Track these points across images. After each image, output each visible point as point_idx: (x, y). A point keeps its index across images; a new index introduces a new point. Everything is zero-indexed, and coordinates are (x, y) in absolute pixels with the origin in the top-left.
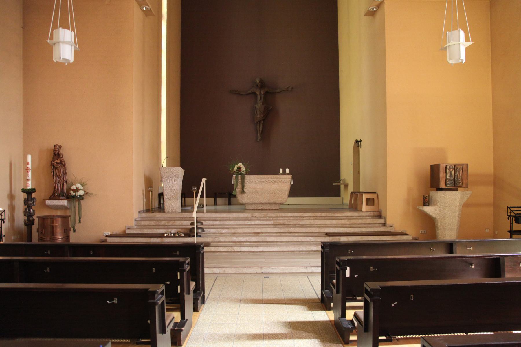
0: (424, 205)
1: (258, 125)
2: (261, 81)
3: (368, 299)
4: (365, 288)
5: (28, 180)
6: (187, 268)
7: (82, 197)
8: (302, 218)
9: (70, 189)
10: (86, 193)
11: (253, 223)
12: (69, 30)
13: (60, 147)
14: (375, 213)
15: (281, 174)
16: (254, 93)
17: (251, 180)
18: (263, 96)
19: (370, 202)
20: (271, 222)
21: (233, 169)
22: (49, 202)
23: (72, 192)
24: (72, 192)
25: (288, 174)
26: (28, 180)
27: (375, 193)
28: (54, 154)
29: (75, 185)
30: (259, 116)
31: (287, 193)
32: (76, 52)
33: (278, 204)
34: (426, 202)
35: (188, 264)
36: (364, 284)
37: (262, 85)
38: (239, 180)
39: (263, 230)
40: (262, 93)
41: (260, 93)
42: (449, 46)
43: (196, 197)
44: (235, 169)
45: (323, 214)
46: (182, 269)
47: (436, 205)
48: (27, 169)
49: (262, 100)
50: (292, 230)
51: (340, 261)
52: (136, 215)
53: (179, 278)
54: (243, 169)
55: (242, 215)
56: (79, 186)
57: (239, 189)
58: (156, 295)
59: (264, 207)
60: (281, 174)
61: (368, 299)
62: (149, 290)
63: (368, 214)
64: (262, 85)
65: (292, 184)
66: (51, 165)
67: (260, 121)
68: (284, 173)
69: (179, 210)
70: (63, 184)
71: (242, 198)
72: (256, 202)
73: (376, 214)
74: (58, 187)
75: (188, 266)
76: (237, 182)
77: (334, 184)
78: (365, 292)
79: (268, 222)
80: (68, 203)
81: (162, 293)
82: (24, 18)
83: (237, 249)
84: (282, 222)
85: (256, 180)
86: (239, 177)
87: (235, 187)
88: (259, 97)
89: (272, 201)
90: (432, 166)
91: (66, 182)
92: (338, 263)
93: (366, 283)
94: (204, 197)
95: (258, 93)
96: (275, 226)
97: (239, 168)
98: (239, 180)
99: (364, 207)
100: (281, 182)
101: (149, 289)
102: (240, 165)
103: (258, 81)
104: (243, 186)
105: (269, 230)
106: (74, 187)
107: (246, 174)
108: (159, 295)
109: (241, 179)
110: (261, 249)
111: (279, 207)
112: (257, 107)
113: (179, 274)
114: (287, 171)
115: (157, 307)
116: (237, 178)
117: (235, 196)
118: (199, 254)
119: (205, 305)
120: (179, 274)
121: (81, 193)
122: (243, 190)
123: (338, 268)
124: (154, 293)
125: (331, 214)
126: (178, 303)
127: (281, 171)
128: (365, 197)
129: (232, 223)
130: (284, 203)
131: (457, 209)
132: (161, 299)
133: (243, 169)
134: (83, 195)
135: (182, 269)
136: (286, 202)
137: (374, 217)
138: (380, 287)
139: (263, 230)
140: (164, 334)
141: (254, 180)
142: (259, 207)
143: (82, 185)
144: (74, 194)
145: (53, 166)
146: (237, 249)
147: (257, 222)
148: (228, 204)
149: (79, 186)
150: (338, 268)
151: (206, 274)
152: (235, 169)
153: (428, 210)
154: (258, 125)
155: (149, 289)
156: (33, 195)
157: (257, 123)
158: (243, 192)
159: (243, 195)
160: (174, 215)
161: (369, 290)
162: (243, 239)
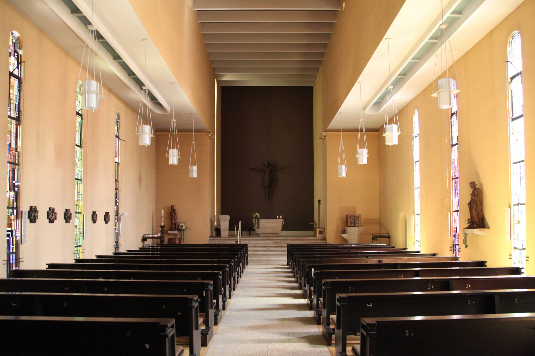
0: (342, 234)
1: (266, 189)
2: (268, 163)
3: (365, 333)
4: (337, 298)
5: (162, 222)
6: (211, 288)
7: (184, 230)
8: (287, 240)
9: (178, 226)
10: (186, 228)
11: (263, 242)
12: (148, 125)
13: (174, 206)
14: (323, 238)
15: (278, 218)
16: (264, 170)
17: (263, 222)
18: (269, 172)
19: (321, 232)
20: (272, 242)
21: (253, 216)
22: (169, 232)
23: (180, 227)
24: (180, 227)
25: (281, 218)
26: (162, 222)
27: (324, 228)
28: (172, 209)
29: (181, 224)
30: (266, 184)
31: (280, 228)
32: (179, 159)
33: (276, 234)
34: (344, 232)
35: (211, 285)
36: (336, 295)
37: (269, 165)
38: (257, 222)
39: (268, 245)
40: (269, 170)
41: (267, 170)
42: (387, 134)
43: (237, 230)
44: (255, 216)
45: (297, 238)
46: (191, 305)
47: (347, 233)
48: (162, 217)
49: (269, 174)
50: (281, 245)
51: (340, 297)
52: (208, 239)
53: (204, 295)
54: (259, 216)
55: (258, 238)
56: (183, 224)
57: (256, 226)
58: (167, 329)
59: (269, 235)
60: (278, 218)
61: (365, 333)
62: (160, 324)
63: (319, 238)
64: (269, 165)
65: (283, 223)
66: (170, 215)
67: (267, 187)
68: (279, 218)
69: (228, 236)
70: (176, 224)
71: (258, 231)
72: (265, 233)
73: (323, 238)
74: (173, 225)
75: (196, 303)
76: (255, 223)
77: (309, 223)
78: (362, 328)
79: (271, 242)
80: (178, 232)
81: (172, 327)
82: (156, 144)
83: (256, 253)
84: (277, 242)
85: (265, 222)
86: (257, 220)
87: (254, 225)
88: (267, 172)
89: (273, 233)
90: (346, 215)
91: (177, 222)
92: (338, 300)
93: (338, 294)
94: (235, 231)
95: (266, 170)
96: (274, 243)
97: (257, 216)
98: (257, 222)
99: (318, 235)
100: (277, 222)
101: (160, 323)
102: (257, 214)
103: (266, 163)
104: (258, 225)
105: (271, 245)
106: (181, 225)
107: (260, 218)
108: (169, 328)
109: (258, 221)
110: (267, 253)
111: (276, 235)
112: (265, 178)
113: (204, 292)
114: (281, 217)
115: (167, 339)
116: (255, 220)
117: (254, 230)
118: (218, 280)
119: (248, 265)
120: (204, 292)
121: (184, 228)
122: (258, 227)
123: (339, 304)
124: (165, 327)
125: (301, 238)
126: (187, 335)
127: (278, 217)
128: (318, 230)
129: (254, 242)
130: (278, 233)
131: (357, 235)
132: (171, 332)
133: (259, 216)
134: (185, 229)
135: (191, 305)
136: (280, 233)
137: (322, 240)
138: (376, 322)
139: (268, 245)
140: (197, 331)
141: (264, 222)
142: (267, 235)
143: (184, 224)
144: (181, 228)
145: (172, 215)
146: (256, 253)
147: (266, 242)
148: (249, 234)
149: (183, 224)
150: (339, 304)
151: (249, 254)
152: (255, 216)
153: (344, 236)
154: (266, 189)
155: (160, 323)
156: (164, 228)
157: (265, 188)
158: (258, 227)
159: (259, 229)
160: (226, 239)
161: (365, 324)
162: (259, 249)
